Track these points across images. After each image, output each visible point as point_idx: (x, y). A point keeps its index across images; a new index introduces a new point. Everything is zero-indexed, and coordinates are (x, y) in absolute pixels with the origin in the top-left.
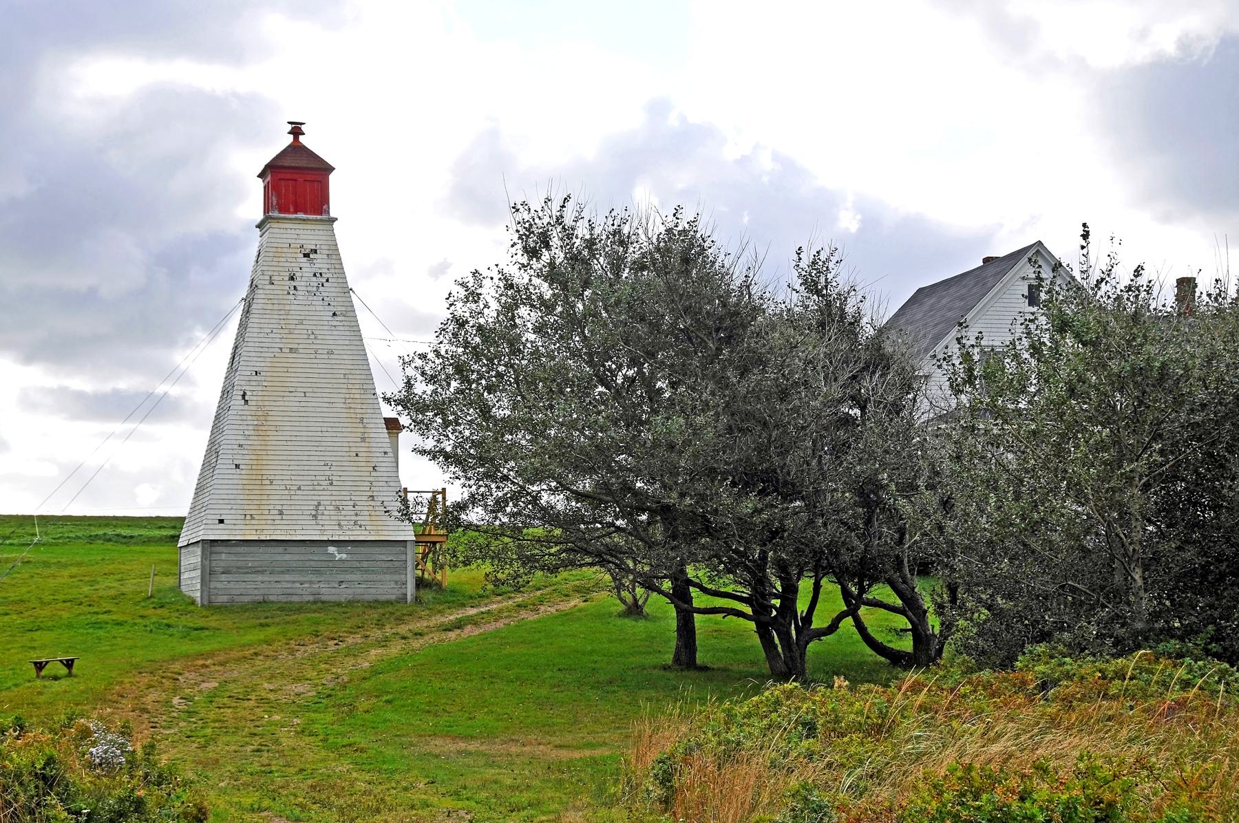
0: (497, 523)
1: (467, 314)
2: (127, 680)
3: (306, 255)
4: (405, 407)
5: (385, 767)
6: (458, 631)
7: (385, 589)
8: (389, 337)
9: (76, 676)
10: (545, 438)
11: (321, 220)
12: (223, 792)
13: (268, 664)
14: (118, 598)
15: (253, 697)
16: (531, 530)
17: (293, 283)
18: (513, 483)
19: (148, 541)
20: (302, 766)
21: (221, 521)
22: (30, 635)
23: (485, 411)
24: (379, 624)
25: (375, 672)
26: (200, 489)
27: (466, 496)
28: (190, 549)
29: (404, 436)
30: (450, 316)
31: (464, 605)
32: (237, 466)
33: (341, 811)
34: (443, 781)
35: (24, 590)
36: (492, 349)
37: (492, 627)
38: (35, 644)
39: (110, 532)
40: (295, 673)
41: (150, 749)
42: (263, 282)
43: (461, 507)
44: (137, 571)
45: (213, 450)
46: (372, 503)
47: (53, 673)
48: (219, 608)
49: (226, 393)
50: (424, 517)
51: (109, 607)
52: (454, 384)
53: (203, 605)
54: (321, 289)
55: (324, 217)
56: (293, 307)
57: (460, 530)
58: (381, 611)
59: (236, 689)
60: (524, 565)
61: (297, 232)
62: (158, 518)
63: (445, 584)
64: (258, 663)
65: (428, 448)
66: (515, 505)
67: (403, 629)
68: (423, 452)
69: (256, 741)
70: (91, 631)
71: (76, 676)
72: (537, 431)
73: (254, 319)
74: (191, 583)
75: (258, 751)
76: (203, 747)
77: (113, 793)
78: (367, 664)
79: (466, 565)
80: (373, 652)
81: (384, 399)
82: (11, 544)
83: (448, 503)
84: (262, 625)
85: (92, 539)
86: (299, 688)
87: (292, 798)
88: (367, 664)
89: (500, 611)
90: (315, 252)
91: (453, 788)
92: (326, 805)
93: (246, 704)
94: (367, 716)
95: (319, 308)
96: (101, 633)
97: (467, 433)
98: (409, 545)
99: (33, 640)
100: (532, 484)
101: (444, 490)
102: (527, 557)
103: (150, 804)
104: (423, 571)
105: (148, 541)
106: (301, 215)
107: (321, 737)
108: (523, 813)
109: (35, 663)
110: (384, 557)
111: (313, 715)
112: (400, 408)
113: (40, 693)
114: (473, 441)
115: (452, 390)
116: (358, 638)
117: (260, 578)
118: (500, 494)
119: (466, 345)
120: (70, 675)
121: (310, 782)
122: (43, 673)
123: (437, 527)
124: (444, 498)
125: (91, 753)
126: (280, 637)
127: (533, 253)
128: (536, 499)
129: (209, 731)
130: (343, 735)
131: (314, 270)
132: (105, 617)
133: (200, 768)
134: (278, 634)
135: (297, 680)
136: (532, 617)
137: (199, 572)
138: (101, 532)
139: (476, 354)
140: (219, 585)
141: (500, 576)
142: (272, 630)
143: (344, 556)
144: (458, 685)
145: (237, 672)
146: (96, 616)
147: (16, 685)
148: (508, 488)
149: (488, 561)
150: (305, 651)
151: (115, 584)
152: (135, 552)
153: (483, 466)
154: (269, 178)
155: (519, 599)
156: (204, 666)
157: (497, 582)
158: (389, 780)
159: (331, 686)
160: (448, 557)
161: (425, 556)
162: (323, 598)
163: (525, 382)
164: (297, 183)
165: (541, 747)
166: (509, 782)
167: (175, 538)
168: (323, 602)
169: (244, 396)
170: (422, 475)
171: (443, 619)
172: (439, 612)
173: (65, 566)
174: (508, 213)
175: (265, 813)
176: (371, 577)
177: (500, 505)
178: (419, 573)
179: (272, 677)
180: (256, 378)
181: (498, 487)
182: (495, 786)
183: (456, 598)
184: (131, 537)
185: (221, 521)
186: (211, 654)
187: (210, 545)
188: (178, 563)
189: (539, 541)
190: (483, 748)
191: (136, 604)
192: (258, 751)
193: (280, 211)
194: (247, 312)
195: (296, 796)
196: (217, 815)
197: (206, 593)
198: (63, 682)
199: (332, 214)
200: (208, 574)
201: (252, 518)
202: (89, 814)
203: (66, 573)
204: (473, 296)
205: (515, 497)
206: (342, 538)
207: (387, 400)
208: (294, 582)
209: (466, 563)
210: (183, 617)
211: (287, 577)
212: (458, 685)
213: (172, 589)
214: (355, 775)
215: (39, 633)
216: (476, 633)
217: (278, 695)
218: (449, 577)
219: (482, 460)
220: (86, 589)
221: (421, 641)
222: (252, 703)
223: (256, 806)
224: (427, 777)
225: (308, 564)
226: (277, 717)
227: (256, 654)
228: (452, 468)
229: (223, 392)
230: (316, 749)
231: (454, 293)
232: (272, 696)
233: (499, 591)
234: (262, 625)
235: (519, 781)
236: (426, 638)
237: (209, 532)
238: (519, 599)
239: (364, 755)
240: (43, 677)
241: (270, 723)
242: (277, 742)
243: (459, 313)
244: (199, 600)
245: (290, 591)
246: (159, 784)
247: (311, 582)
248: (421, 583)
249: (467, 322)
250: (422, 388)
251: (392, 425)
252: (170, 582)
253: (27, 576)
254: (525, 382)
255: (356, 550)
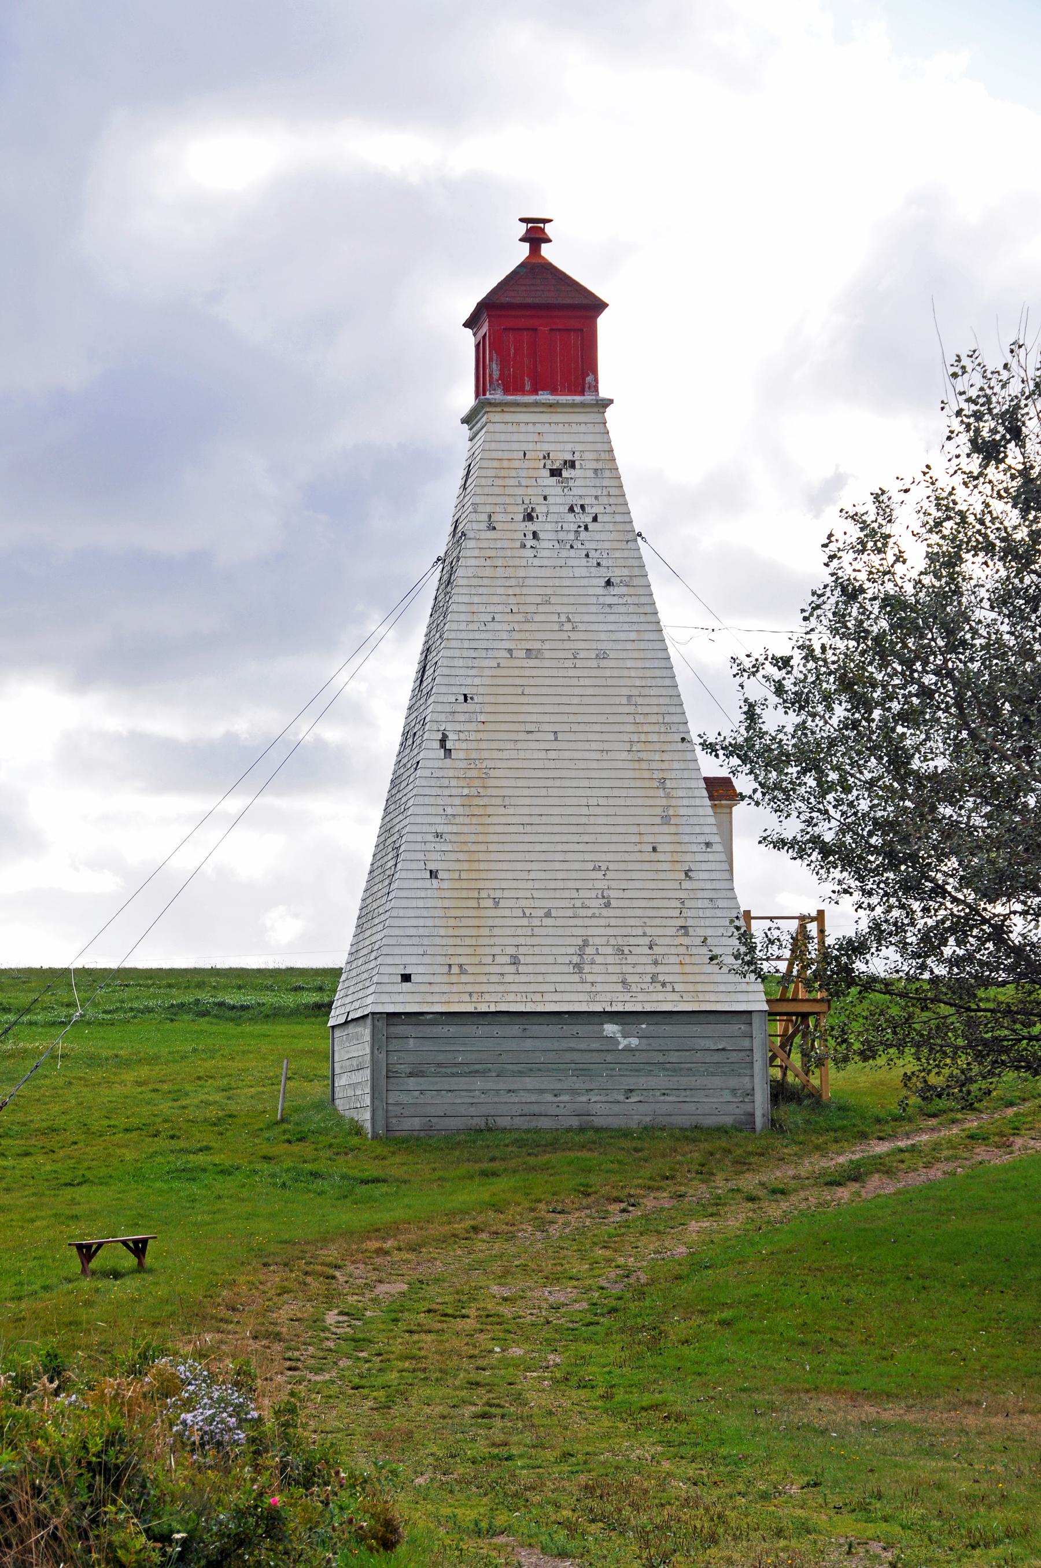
0: (926, 976)
1: (863, 576)
2: (242, 1279)
3: (555, 473)
4: (745, 759)
5: (723, 1451)
6: (855, 1186)
7: (713, 1101)
8: (716, 625)
9: (150, 1271)
10: (1015, 811)
11: (582, 405)
12: (422, 1495)
13: (497, 1247)
14: (223, 1123)
15: (473, 1313)
16: (992, 991)
17: (531, 527)
18: (955, 900)
19: (276, 1014)
20: (567, 1448)
21: (406, 978)
22: (68, 1193)
23: (898, 761)
24: (704, 1172)
25: (698, 1265)
26: (366, 919)
27: (864, 927)
28: (351, 1029)
29: (741, 811)
30: (830, 580)
31: (863, 1136)
32: (433, 874)
33: (644, 1538)
34: (836, 1483)
35: (56, 1108)
36: (911, 642)
37: (919, 1178)
38: (77, 1210)
39: (206, 997)
40: (548, 1266)
41: (288, 1413)
42: (474, 526)
43: (856, 947)
44: (253, 1069)
45: (389, 843)
46: (686, 941)
47: (109, 1265)
48: (406, 1140)
49: (410, 737)
50: (783, 966)
51: (209, 1139)
52: (840, 711)
53: (375, 1136)
54: (583, 535)
55: (588, 398)
56: (533, 572)
57: (854, 990)
58: (706, 1146)
59: (441, 1296)
60: (979, 1056)
61: (538, 428)
62: (291, 971)
63: (828, 1094)
64: (479, 1246)
65: (788, 836)
66: (959, 943)
67: (749, 1182)
68: (780, 844)
69: (480, 1397)
70: (176, 1184)
71: (150, 1271)
72: (1003, 797)
73: (459, 596)
74: (354, 1092)
75: (484, 1416)
76: (383, 1408)
77: (225, 1499)
78: (683, 1249)
79: (865, 1059)
80: (693, 1225)
81: (705, 745)
82: (31, 1023)
83: (830, 941)
84: (484, 1174)
85: (175, 1011)
86: (558, 1294)
87: (550, 1509)
88: (683, 1249)
89: (936, 1147)
90: (572, 465)
91: (856, 1497)
92: (615, 1525)
93: (460, 1324)
94: (685, 1350)
95: (578, 572)
96: (194, 1188)
97: (864, 806)
98: (756, 1020)
99: (73, 1202)
100: (992, 901)
101: (821, 913)
102: (985, 1043)
103: (294, 1523)
104: (784, 1069)
105: (276, 1014)
106: (544, 397)
107: (600, 1391)
108: (994, 1552)
109: (80, 1247)
110: (710, 1044)
111: (585, 1348)
112: (735, 761)
113: (88, 1304)
114: (875, 821)
115: (835, 721)
116: (663, 1200)
117: (479, 1083)
118: (931, 922)
119: (861, 634)
120: (141, 1268)
121: (583, 1479)
122: (93, 1264)
123: (808, 984)
124: (822, 931)
125: (184, 1423)
126: (519, 1197)
127: (989, 451)
128: (999, 932)
129: (393, 1376)
130: (644, 1389)
131: (570, 501)
132: (201, 1159)
133: (379, 1447)
134: (515, 1190)
135: (552, 1279)
136: (999, 1159)
137: (367, 1073)
138: (188, 999)
139: (881, 648)
140: (404, 1098)
141: (933, 1079)
142: (502, 1185)
143: (634, 1042)
144: (857, 1292)
145: (446, 1262)
146: (185, 1158)
147: (45, 1288)
148: (946, 910)
149: (910, 1050)
150: (566, 1224)
151: (217, 1097)
152: (253, 1036)
153: (894, 867)
154: (485, 329)
155: (973, 1124)
156: (380, 1252)
157: (928, 1093)
158: (733, 1477)
159: (616, 1291)
160: (832, 1043)
161: (787, 1040)
162: (598, 1122)
163: (975, 702)
164: (538, 333)
165: (1026, 1418)
166: (964, 1487)
167: (325, 1008)
168: (598, 1130)
169: (443, 741)
170: (782, 885)
171: (824, 1163)
172: (817, 1148)
173: (126, 1064)
174: (941, 377)
175: (502, 1540)
176: (684, 1081)
177: (930, 943)
178: (777, 1073)
179: (506, 1273)
180: (465, 707)
181: (926, 910)
182: (938, 1495)
183: (847, 1122)
184: (243, 1008)
185: (406, 978)
186: (392, 1230)
187: (388, 1023)
188: (329, 1057)
189: (1008, 1012)
190: (909, 1418)
191: (256, 1133)
192: (484, 1416)
193: (506, 391)
194: (447, 583)
195: (557, 1506)
196: (413, 1541)
197: (380, 1113)
198: (128, 1281)
199: (604, 392)
200: (384, 1077)
201: (462, 970)
202: (184, 1542)
203: (129, 1076)
204: (873, 538)
205: (960, 928)
206: (629, 1008)
207: (710, 748)
208: (542, 1091)
209: (868, 1054)
210: (341, 1159)
211: (529, 1082)
212: (857, 1292)
213: (319, 1106)
214: (666, 1466)
215: (84, 1188)
216: (890, 1190)
217: (519, 1309)
218: (839, 1081)
219: (893, 860)
220: (165, 1107)
221: (784, 1205)
222: (470, 1324)
223: (484, 1525)
224: (805, 1472)
225: (568, 1056)
226: (516, 1352)
227: (475, 1229)
228: (836, 873)
229: (405, 735)
230: (591, 1414)
231: (838, 535)
232: (506, 1310)
233: (932, 1108)
234: (484, 1174)
235: (984, 1486)
236: (793, 1198)
237: (385, 998)
238: (973, 1124)
239: (683, 1427)
240: (94, 1273)
241: (506, 1363)
242: (519, 1399)
243: (847, 572)
244: (368, 1125)
245: (536, 1109)
246: (307, 1484)
247: (573, 1092)
248: (780, 1093)
249: (862, 590)
250: (778, 721)
251: (720, 791)
252: (317, 1090)
253: (61, 1082)
254: (975, 702)
255: (655, 1030)
